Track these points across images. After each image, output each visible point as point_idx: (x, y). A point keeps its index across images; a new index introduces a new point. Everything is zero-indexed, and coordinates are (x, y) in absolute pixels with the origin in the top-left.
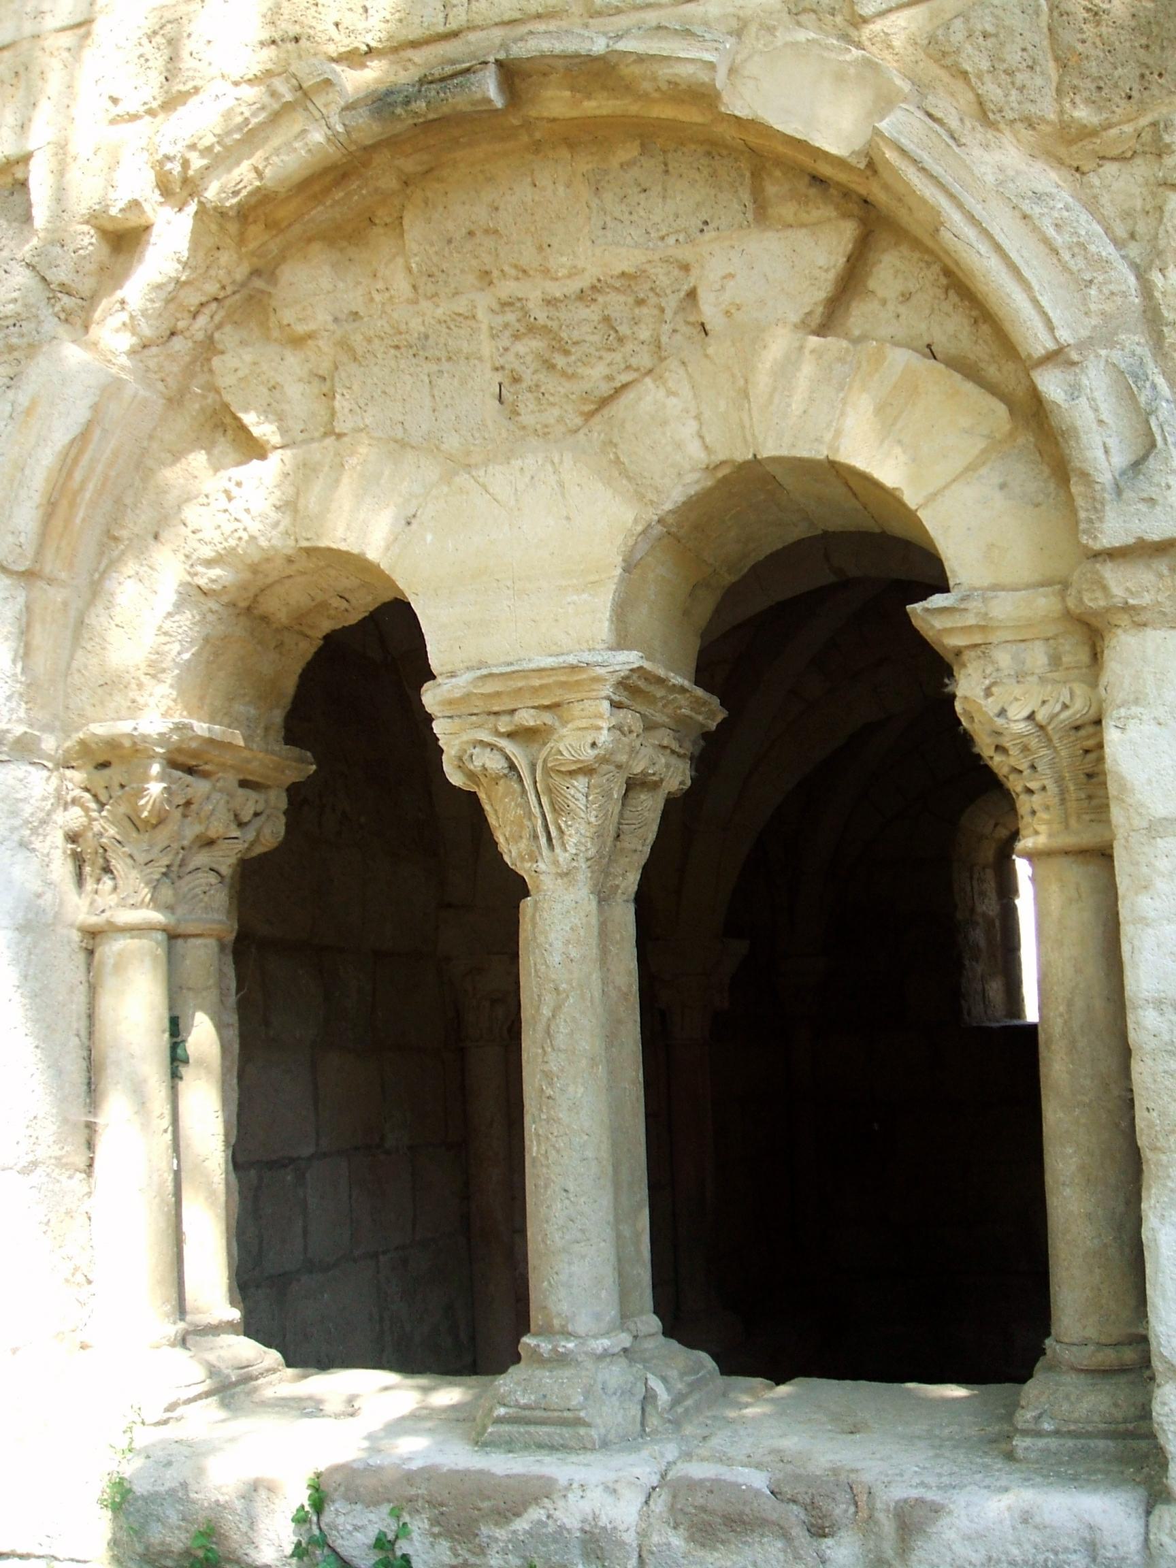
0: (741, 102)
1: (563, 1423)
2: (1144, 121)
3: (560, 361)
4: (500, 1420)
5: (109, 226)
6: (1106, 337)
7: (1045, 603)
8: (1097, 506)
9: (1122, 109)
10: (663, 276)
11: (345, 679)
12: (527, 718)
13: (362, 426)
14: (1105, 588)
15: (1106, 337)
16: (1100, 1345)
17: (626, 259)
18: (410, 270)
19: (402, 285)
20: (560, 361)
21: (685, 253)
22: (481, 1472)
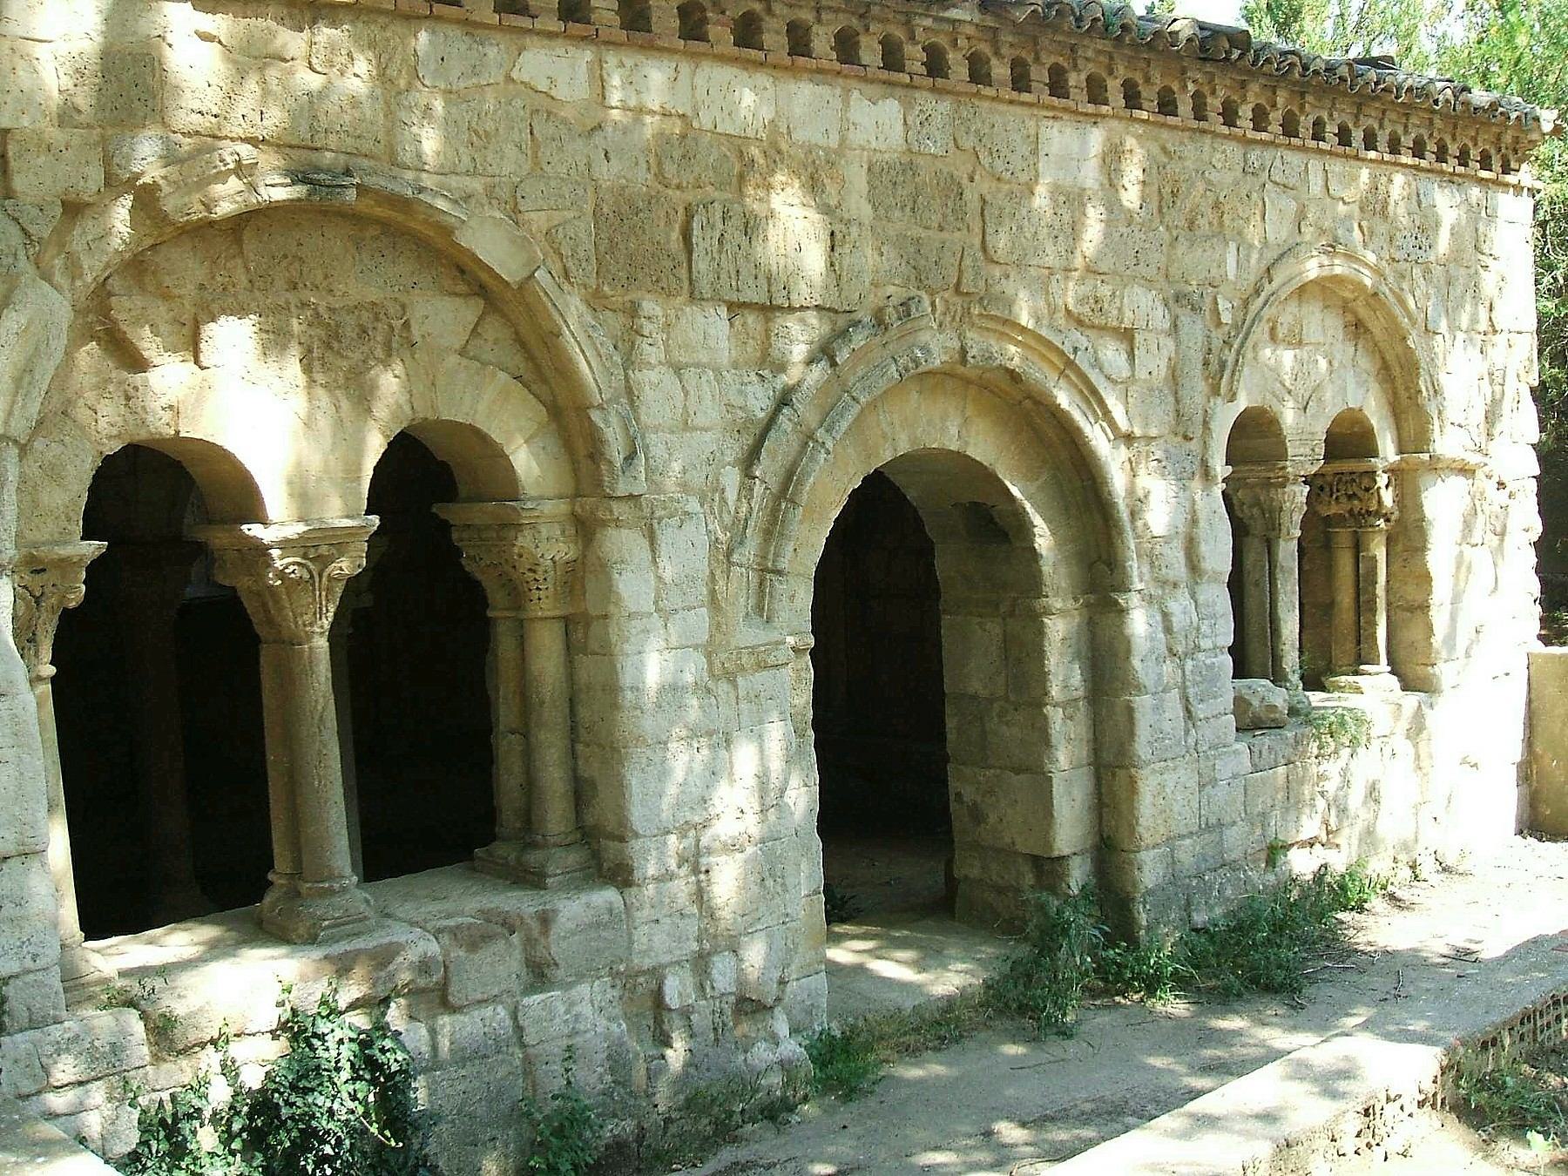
0: (465, 239)
1: (360, 920)
2: (627, 298)
3: (336, 345)
4: (328, 927)
5: (87, 212)
6: (615, 400)
7: (563, 507)
8: (615, 479)
9: (620, 290)
10: (393, 310)
11: (160, 503)
12: (324, 550)
13: (735, 558)
14: (611, 512)
15: (615, 400)
16: (566, 834)
17: (373, 294)
18: (248, 270)
19: (242, 279)
20: (336, 345)
21: (403, 298)
22: (1294, 1028)
